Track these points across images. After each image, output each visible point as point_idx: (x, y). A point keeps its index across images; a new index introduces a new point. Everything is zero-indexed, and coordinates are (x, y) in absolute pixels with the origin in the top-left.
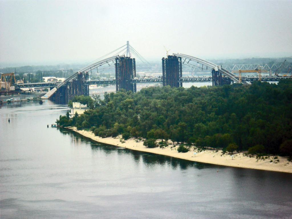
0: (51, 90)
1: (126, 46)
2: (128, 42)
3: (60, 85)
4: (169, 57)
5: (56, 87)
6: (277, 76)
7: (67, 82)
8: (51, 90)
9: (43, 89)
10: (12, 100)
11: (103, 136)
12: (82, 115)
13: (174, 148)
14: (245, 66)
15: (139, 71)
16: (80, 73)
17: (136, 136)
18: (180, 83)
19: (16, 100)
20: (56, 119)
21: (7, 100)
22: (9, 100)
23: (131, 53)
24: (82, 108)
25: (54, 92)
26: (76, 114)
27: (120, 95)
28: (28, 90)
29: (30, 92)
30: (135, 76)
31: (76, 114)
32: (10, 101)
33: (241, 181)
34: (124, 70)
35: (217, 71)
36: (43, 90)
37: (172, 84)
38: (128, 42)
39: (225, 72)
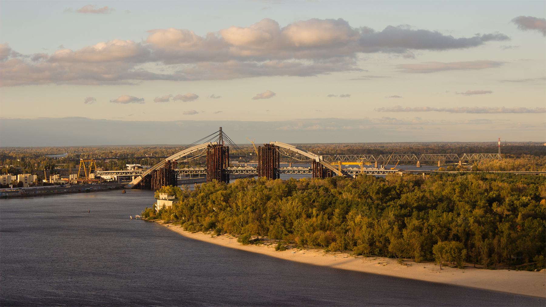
0: (135, 179)
1: (219, 133)
2: (221, 128)
3: (146, 173)
4: (267, 145)
5: (141, 176)
6: (384, 169)
7: (154, 170)
8: (135, 179)
9: (126, 177)
10: (92, 188)
11: (194, 231)
12: (170, 207)
13: (270, 246)
14: (348, 158)
15: (232, 161)
16: (168, 160)
17: (232, 233)
18: (277, 175)
19: (96, 189)
20: (163, 204)
21: (86, 189)
22: (89, 189)
23: (224, 140)
24: (170, 200)
25: (138, 181)
26: (164, 206)
27: (162, 218)
28: (110, 178)
29: (111, 180)
30: (229, 166)
31: (164, 206)
32: (89, 190)
33: (186, 195)
34: (216, 159)
35: (318, 162)
36: (127, 178)
37: (269, 176)
38: (221, 128)
39: (315, 167)
